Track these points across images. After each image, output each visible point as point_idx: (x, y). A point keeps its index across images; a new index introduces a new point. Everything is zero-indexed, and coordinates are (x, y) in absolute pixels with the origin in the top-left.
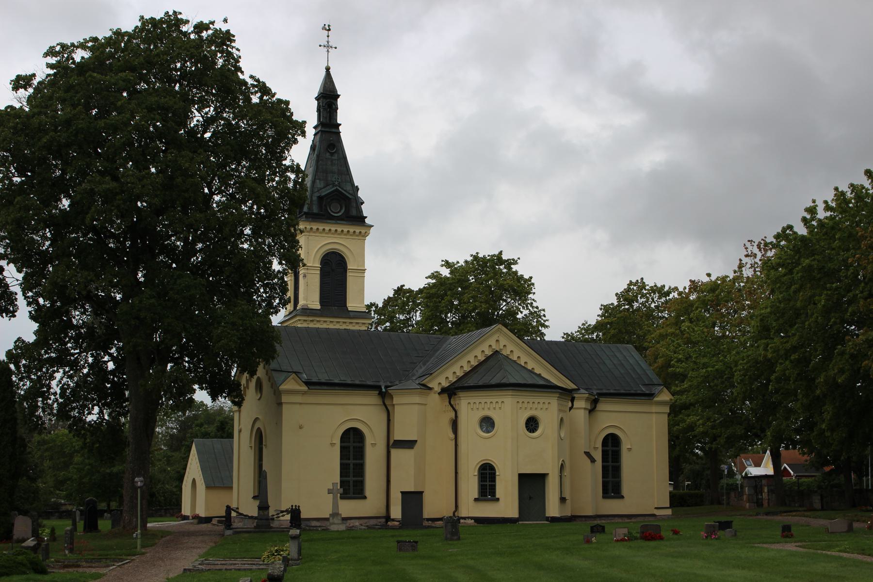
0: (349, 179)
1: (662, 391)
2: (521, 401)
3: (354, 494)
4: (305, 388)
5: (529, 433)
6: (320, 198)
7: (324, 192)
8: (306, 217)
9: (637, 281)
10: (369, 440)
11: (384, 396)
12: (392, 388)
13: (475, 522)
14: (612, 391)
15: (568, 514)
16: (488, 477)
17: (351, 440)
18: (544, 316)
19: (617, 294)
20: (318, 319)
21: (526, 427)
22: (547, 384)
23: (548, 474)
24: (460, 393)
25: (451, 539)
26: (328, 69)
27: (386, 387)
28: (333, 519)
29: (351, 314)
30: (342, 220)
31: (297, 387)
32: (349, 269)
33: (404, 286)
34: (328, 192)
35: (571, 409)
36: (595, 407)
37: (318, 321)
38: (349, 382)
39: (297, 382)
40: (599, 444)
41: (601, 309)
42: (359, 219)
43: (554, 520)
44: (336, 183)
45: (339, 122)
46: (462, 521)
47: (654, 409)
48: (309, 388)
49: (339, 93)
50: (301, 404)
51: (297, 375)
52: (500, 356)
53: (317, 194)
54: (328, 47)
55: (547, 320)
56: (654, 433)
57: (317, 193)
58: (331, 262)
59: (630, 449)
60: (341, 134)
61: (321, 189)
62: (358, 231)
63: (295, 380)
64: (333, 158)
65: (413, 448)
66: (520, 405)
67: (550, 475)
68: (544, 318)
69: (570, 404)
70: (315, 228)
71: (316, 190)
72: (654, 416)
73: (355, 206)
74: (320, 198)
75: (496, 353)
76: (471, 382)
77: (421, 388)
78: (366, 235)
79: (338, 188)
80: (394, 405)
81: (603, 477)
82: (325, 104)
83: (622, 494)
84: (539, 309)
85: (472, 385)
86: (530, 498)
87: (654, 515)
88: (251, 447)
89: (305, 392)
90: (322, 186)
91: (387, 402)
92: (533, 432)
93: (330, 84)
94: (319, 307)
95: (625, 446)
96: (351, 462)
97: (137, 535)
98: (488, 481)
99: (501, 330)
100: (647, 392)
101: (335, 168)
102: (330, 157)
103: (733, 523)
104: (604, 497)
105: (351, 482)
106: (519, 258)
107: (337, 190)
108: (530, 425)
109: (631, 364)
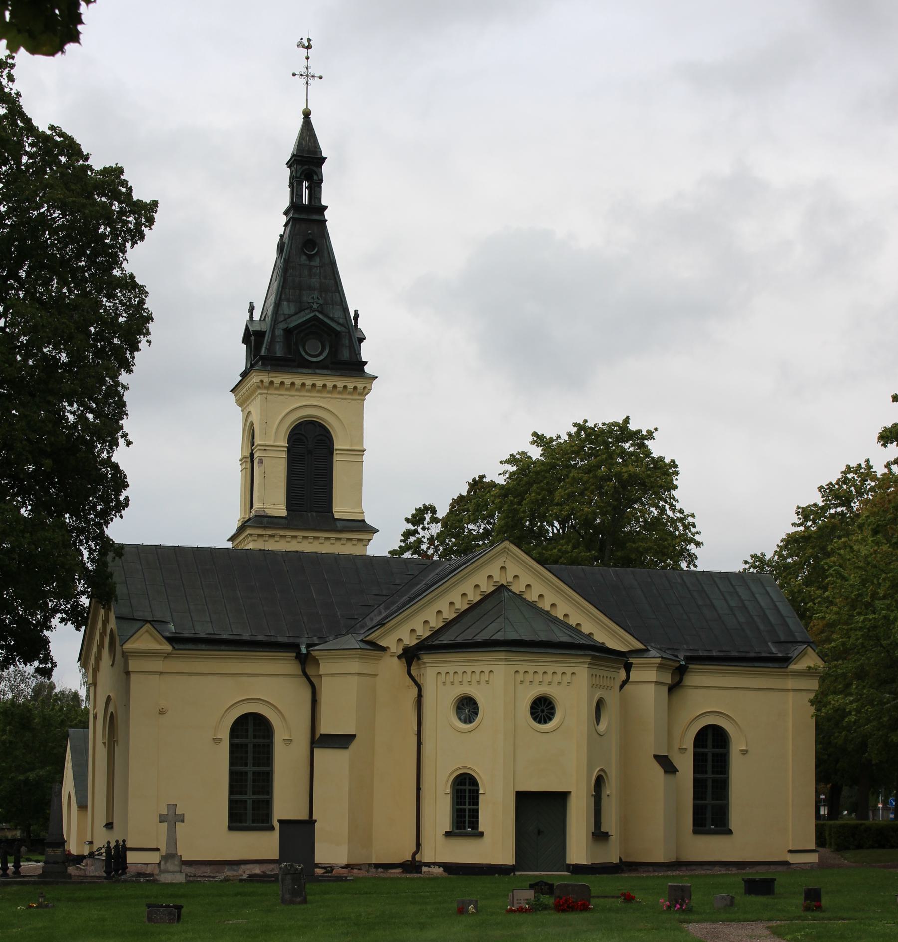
0: (339, 299)
1: (805, 654)
2: (522, 669)
3: (253, 822)
4: (167, 647)
5: (532, 720)
6: (288, 332)
7: (294, 322)
8: (263, 364)
9: (859, 465)
10: (280, 735)
11: (305, 661)
12: (316, 648)
13: (444, 871)
14: (715, 654)
15: (614, 858)
16: (467, 798)
18: (694, 526)
19: (821, 488)
20: (282, 533)
21: (532, 714)
22: (572, 641)
25: (292, 902)
26: (307, 114)
27: (309, 646)
28: (165, 863)
29: (339, 524)
31: (153, 646)
32: (336, 450)
33: (484, 476)
34: (304, 319)
36: (681, 680)
37: (282, 536)
38: (246, 637)
39: (155, 639)
40: (689, 743)
41: (798, 513)
43: (578, 869)
45: (324, 203)
46: (424, 869)
47: (791, 683)
48: (173, 647)
49: (324, 155)
50: (161, 673)
52: (506, 594)
53: (283, 326)
54: (307, 76)
55: (698, 533)
56: (790, 724)
57: (283, 323)
58: (306, 438)
59: (745, 752)
60: (327, 223)
61: (290, 316)
62: (350, 386)
63: (151, 635)
64: (312, 264)
65: (347, 748)
66: (520, 677)
67: (572, 793)
68: (693, 530)
69: (623, 674)
71: (282, 319)
72: (791, 694)
73: (347, 345)
74: (288, 332)
75: (502, 589)
76: (445, 639)
77: (361, 649)
78: (365, 392)
79: (317, 314)
80: (320, 676)
82: (301, 174)
83: (730, 828)
84: (685, 514)
85: (445, 642)
86: (539, 833)
87: (786, 863)
88: (104, 743)
89: (168, 654)
90: (292, 311)
91: (310, 671)
92: (545, 722)
93: (310, 140)
94: (284, 513)
95: (736, 746)
96: (250, 769)
99: (508, 549)
100: (780, 655)
101: (315, 282)
102: (308, 262)
103: (776, 882)
104: (696, 832)
105: (249, 802)
106: (656, 429)
107: (315, 318)
108: (546, 711)
109: (761, 607)
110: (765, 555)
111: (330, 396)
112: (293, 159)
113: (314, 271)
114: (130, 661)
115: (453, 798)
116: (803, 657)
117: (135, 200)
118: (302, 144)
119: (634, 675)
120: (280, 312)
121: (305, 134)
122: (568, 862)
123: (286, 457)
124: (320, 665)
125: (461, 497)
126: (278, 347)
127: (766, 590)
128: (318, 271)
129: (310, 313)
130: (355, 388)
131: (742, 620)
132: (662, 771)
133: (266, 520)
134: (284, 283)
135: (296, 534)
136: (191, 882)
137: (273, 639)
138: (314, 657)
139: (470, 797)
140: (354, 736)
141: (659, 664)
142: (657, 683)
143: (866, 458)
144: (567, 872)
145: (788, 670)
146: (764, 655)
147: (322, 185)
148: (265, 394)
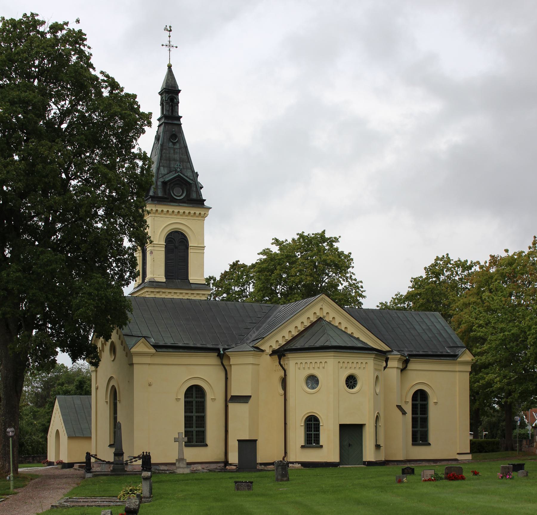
0: (189, 166)
1: (465, 353)
2: (341, 361)
3: (196, 442)
4: (153, 350)
6: (164, 183)
7: (168, 178)
8: (152, 200)
9: (443, 256)
10: (209, 396)
11: (222, 357)
12: (229, 350)
13: (302, 466)
14: (421, 353)
16: (313, 428)
17: (194, 395)
18: (362, 287)
19: (425, 268)
20: (163, 291)
21: (346, 384)
23: (365, 424)
24: (289, 355)
25: (282, 480)
26: (170, 67)
27: (224, 350)
28: (179, 463)
29: (193, 286)
30: (184, 202)
32: (190, 246)
33: (239, 261)
35: (385, 368)
36: (406, 367)
38: (191, 345)
39: (145, 345)
40: (409, 399)
41: (411, 281)
42: (199, 202)
43: (370, 464)
44: (179, 170)
45: (180, 114)
47: (458, 368)
48: (156, 351)
49: (180, 89)
51: (145, 338)
52: (324, 322)
53: (162, 180)
54: (169, 46)
58: (174, 240)
59: (436, 403)
61: (165, 175)
63: (144, 344)
64: (175, 147)
66: (341, 365)
68: (362, 289)
70: (160, 210)
72: (458, 374)
73: (195, 190)
75: (320, 319)
77: (254, 351)
78: (205, 216)
79: (180, 174)
81: (413, 427)
84: (357, 281)
85: (299, 347)
88: (107, 402)
89: (153, 354)
91: (225, 363)
92: (353, 388)
93: (172, 80)
94: (164, 280)
95: (432, 400)
97: (10, 478)
98: (313, 431)
99: (324, 299)
101: (177, 157)
102: (173, 146)
104: (413, 445)
106: (340, 237)
107: (179, 176)
109: (438, 329)
110: (387, 303)
111: (187, 218)
112: (163, 91)
113: (176, 151)
114: (134, 358)
115: (305, 428)
116: (464, 354)
117: (141, 112)
118: (168, 83)
119: (390, 364)
120: (160, 173)
121: (169, 77)
122: (364, 460)
123: (164, 250)
124: (231, 360)
125: (226, 272)
126: (159, 191)
127: (438, 320)
128: (178, 151)
129: (176, 173)
130: (200, 214)
131: (430, 336)
132: (401, 413)
133: (155, 283)
134: (161, 157)
135: (187, 292)
136: (193, 473)
137: (204, 346)
138: (227, 355)
139: (314, 427)
140: (250, 396)
141: (399, 358)
142: (397, 368)
143: (447, 253)
144: (364, 465)
145: (457, 361)
146: (444, 353)
147: (179, 105)
148: (153, 216)
